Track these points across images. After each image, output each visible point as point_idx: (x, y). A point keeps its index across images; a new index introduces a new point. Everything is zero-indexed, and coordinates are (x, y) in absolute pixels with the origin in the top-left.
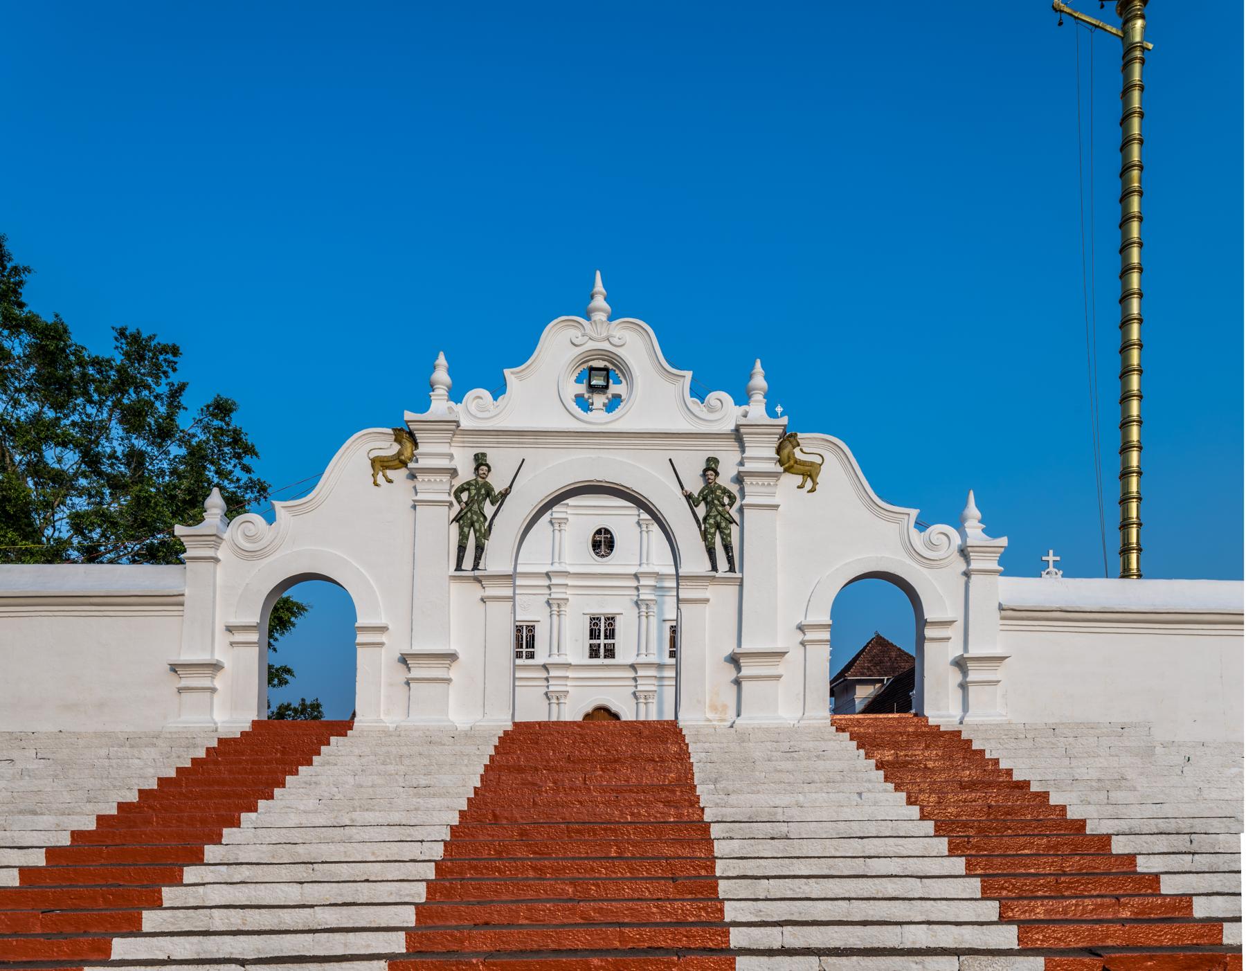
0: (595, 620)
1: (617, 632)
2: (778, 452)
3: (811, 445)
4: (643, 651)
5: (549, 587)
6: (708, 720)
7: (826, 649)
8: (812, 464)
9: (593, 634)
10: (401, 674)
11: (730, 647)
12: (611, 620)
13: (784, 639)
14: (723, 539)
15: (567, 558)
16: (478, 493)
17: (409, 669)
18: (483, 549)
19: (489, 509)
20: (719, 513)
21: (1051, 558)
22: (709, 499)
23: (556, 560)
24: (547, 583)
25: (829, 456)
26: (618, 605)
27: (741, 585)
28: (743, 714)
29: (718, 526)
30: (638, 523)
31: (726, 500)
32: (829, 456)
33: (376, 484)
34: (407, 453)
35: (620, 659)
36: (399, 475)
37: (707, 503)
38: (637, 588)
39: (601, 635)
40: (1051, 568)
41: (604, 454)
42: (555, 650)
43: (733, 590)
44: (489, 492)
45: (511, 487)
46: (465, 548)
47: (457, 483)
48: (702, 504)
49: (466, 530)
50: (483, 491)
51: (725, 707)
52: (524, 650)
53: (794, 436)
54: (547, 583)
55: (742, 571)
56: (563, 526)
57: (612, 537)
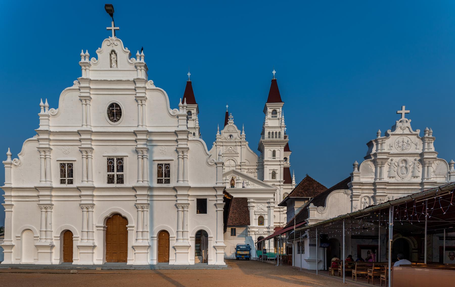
0: (110, 160)
4: (181, 179)
5: (177, 141)
9: (110, 168)
12: (120, 160)
15: (147, 123)
21: (404, 111)
35: (127, 184)
39: (115, 167)
40: (403, 118)
56: (88, 102)
57: (120, 109)
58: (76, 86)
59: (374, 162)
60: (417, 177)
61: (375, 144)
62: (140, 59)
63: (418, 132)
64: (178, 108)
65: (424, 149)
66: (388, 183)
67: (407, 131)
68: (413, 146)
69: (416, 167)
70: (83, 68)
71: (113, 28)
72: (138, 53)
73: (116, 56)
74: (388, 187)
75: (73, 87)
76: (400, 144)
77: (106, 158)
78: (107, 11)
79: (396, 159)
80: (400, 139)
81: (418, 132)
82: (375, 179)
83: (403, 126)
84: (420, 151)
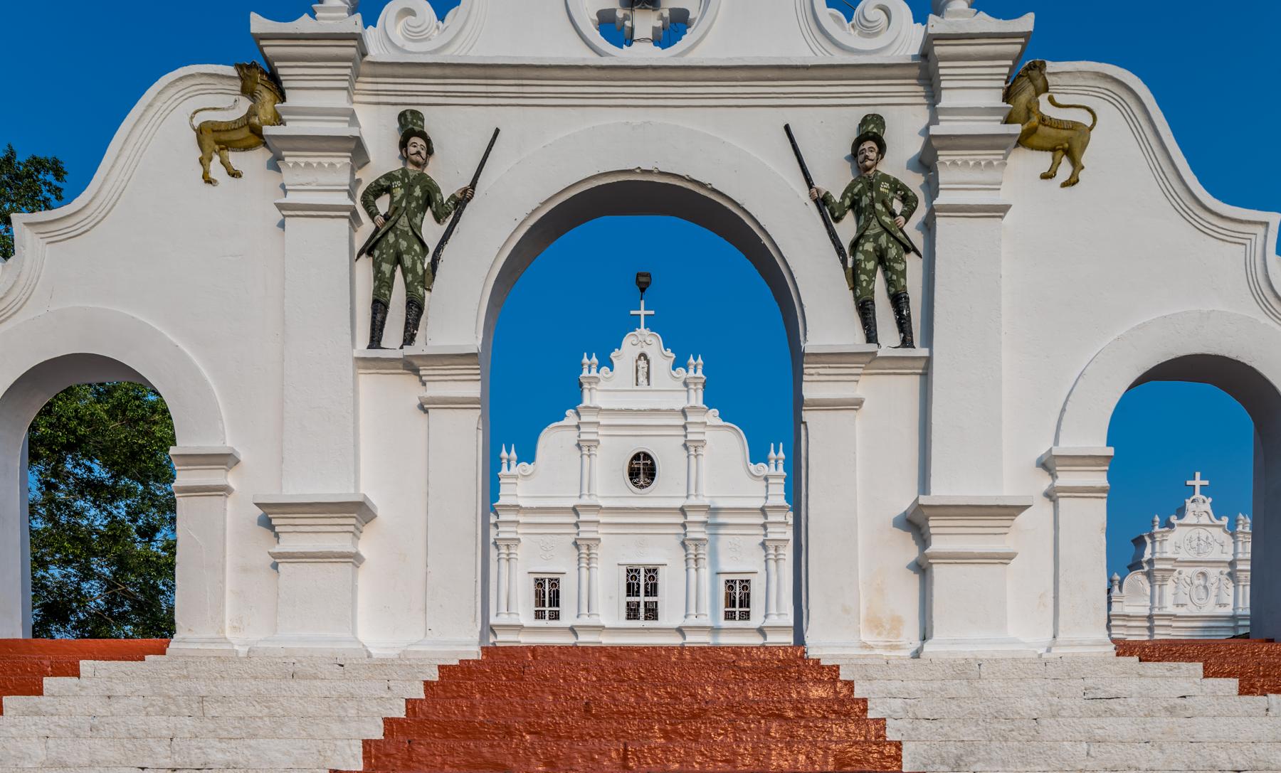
0: (632, 573)
1: (659, 587)
2: (1007, 97)
3: (1074, 87)
5: (577, 525)
6: (865, 646)
7: (1098, 509)
8: (1074, 126)
9: (631, 590)
10: (261, 549)
11: (903, 502)
12: (652, 572)
13: (1014, 480)
14: (889, 282)
15: (598, 489)
16: (408, 195)
17: (277, 535)
18: (420, 309)
19: (431, 230)
20: (886, 229)
21: (1198, 482)
22: (865, 201)
23: (585, 491)
24: (573, 519)
25: (1106, 112)
26: (659, 551)
27: (926, 375)
28: (938, 633)
29: (881, 258)
30: (685, 446)
31: (897, 206)
32: (1106, 112)
33: (209, 181)
34: (265, 112)
36: (251, 161)
37: (858, 213)
38: (684, 526)
40: (1197, 495)
41: (656, 116)
42: (584, 610)
43: (908, 385)
44: (429, 196)
45: (473, 185)
46: (386, 306)
47: (368, 177)
48: (850, 217)
49: (386, 268)
50: (418, 192)
51: (897, 622)
52: (547, 609)
53: (1038, 67)
54: (573, 519)
55: (928, 341)
56: (593, 450)
57: (653, 464)
58: (571, 418)
59: (1149, 575)
60: (1225, 605)
61: (1148, 541)
62: (696, 370)
63: (1225, 520)
64: (767, 462)
65: (1235, 554)
66: (1175, 616)
67: (1204, 520)
68: (1217, 547)
69: (1223, 587)
70: (586, 386)
71: (642, 312)
72: (691, 360)
73: (648, 363)
74: (1174, 624)
75: (565, 422)
76: (1194, 544)
77: (624, 568)
78: (638, 283)
79: (1188, 572)
80: (1194, 533)
81: (1225, 520)
82: (1151, 609)
83: (1199, 508)
84: (1230, 558)
